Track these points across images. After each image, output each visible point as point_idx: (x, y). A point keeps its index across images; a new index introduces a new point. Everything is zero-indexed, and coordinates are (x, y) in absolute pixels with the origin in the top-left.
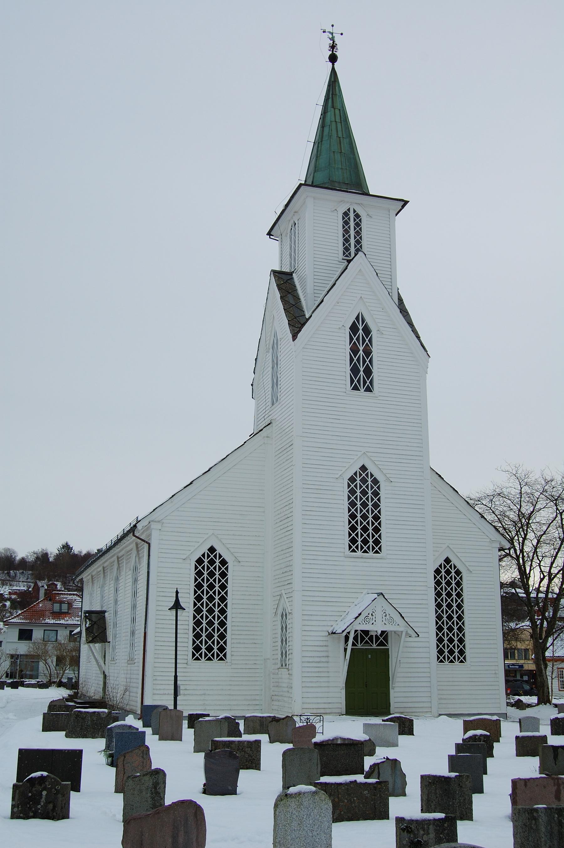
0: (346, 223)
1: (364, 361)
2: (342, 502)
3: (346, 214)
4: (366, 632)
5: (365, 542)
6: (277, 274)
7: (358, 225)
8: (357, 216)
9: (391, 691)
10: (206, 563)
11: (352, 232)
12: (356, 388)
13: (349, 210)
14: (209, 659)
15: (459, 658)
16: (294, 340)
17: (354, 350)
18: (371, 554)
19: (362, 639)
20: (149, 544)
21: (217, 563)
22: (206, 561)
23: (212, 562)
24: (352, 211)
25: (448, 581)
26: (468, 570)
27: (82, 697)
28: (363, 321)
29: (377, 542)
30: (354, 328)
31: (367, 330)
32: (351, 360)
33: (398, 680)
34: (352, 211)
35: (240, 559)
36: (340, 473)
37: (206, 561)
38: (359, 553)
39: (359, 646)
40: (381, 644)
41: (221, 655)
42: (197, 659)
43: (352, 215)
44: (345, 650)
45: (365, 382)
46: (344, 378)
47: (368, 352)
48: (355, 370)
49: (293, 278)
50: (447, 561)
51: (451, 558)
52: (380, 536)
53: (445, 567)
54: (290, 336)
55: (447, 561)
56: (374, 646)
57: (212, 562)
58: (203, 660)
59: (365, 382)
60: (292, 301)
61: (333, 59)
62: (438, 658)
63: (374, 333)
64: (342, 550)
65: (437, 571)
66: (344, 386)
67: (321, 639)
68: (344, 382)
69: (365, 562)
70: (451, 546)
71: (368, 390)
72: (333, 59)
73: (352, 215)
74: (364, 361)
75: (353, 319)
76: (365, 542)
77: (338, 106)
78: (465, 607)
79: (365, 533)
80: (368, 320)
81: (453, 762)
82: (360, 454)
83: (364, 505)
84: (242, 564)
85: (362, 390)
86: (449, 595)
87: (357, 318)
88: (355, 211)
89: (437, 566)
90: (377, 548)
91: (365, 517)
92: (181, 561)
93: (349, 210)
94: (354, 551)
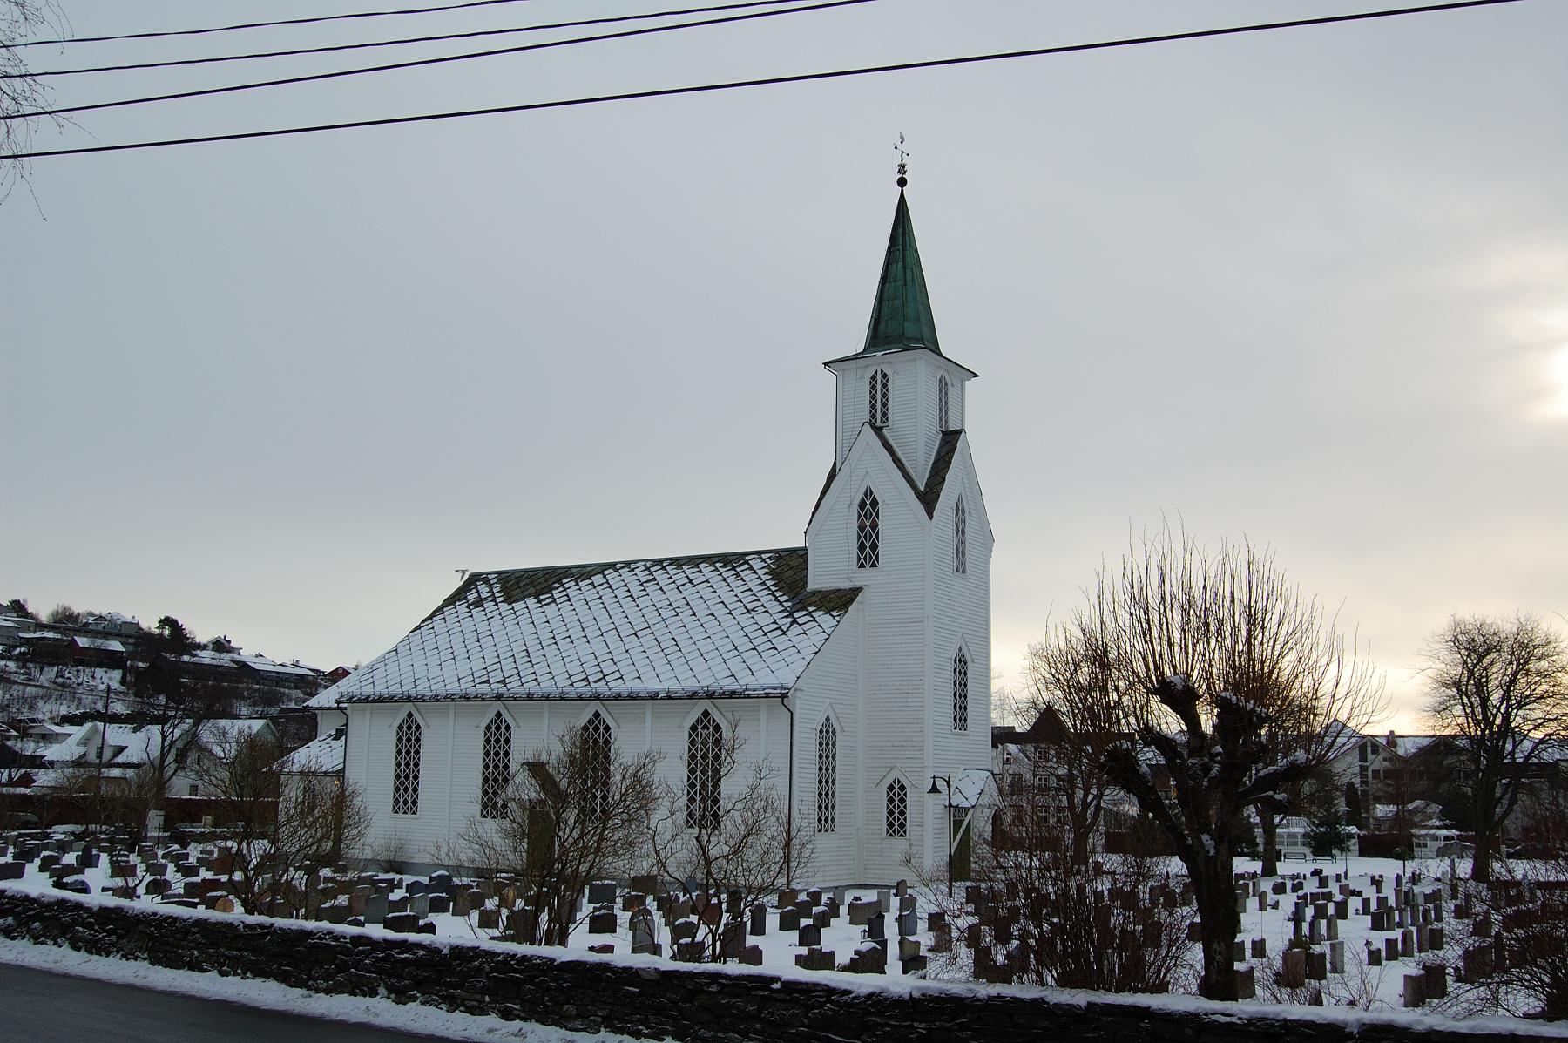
0: (873, 387)
3: (873, 378)
7: (885, 386)
8: (885, 376)
12: (862, 566)
17: (862, 528)
30: (862, 505)
31: (875, 503)
43: (879, 377)
47: (874, 526)
61: (902, 183)
71: (874, 565)
72: (902, 183)
73: (879, 377)
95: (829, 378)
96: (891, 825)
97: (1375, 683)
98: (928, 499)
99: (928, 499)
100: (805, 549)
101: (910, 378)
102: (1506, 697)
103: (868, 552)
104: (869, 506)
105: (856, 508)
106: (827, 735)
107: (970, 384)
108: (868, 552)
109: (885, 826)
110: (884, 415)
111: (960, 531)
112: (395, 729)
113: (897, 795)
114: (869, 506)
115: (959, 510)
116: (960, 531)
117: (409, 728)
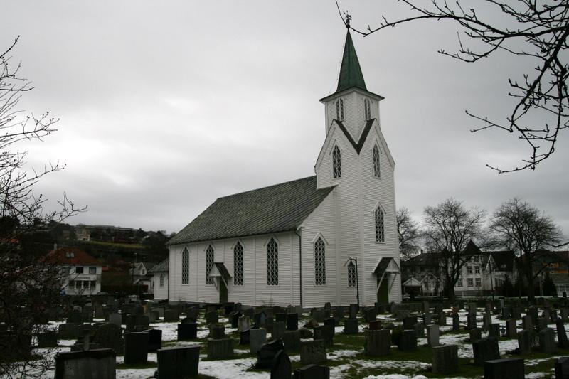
3: (338, 102)
17: (335, 162)
30: (334, 153)
31: (339, 151)
47: (339, 161)
95: (323, 105)
96: (350, 282)
97: (454, 201)
98: (358, 148)
99: (358, 148)
100: (315, 177)
101: (353, 103)
102: (530, 19)
103: (337, 172)
105: (332, 154)
106: (320, 246)
107: (381, 102)
108: (337, 172)
109: (348, 282)
110: (342, 116)
111: (376, 160)
112: (266, 247)
113: (352, 268)
114: (337, 153)
115: (376, 151)
116: (376, 160)
117: (272, 245)
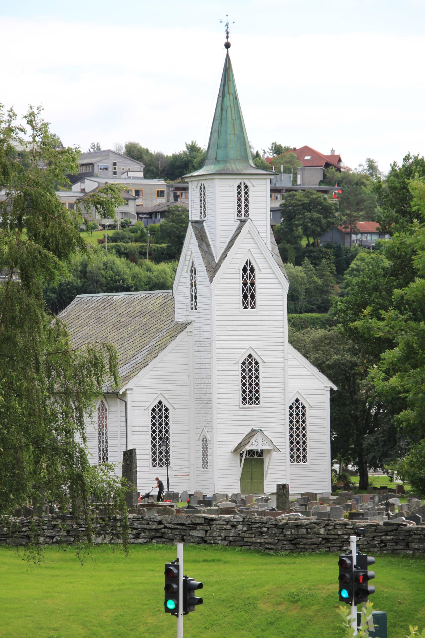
1: (251, 290)
2: (238, 377)
3: (239, 187)
4: (252, 450)
5: (251, 399)
6: (194, 224)
8: (246, 187)
9: (265, 482)
10: (157, 411)
11: (243, 199)
12: (246, 308)
13: (241, 183)
14: (161, 466)
15: (303, 460)
16: (211, 282)
17: (245, 284)
18: (254, 405)
19: (249, 453)
20: (126, 402)
21: (163, 411)
22: (157, 409)
23: (160, 410)
24: (243, 184)
25: (297, 413)
26: (310, 405)
27: (348, 552)
28: (250, 264)
29: (257, 399)
30: (245, 270)
31: (252, 270)
32: (243, 290)
33: (268, 475)
34: (243, 184)
35: (176, 407)
36: (237, 360)
37: (157, 409)
38: (248, 406)
39: (248, 457)
40: (260, 456)
41: (161, 464)
42: (154, 466)
43: (243, 187)
44: (241, 460)
45: (251, 303)
46: (239, 302)
47: (253, 284)
48: (245, 297)
49: (203, 226)
50: (297, 400)
51: (299, 398)
52: (259, 395)
53: (295, 404)
54: (208, 279)
55: (297, 400)
56: (256, 457)
57: (160, 410)
58: (158, 466)
59: (251, 303)
60: (206, 249)
62: (290, 460)
63: (256, 271)
64: (238, 404)
65: (291, 408)
66: (239, 307)
67: (227, 460)
68: (239, 305)
69: (251, 411)
70: (299, 391)
71: (253, 308)
73: (243, 187)
74: (251, 290)
75: (244, 263)
76: (251, 399)
77: (231, 91)
78: (307, 429)
79: (250, 393)
80: (253, 263)
81: (285, 147)
82: (248, 348)
83: (250, 377)
84: (177, 410)
85: (249, 308)
86: (298, 422)
87: (247, 263)
88: (244, 184)
89: (290, 404)
90: (257, 402)
91: (250, 385)
92: (143, 411)
93: (241, 183)
94: (244, 404)
104: (248, 270)
